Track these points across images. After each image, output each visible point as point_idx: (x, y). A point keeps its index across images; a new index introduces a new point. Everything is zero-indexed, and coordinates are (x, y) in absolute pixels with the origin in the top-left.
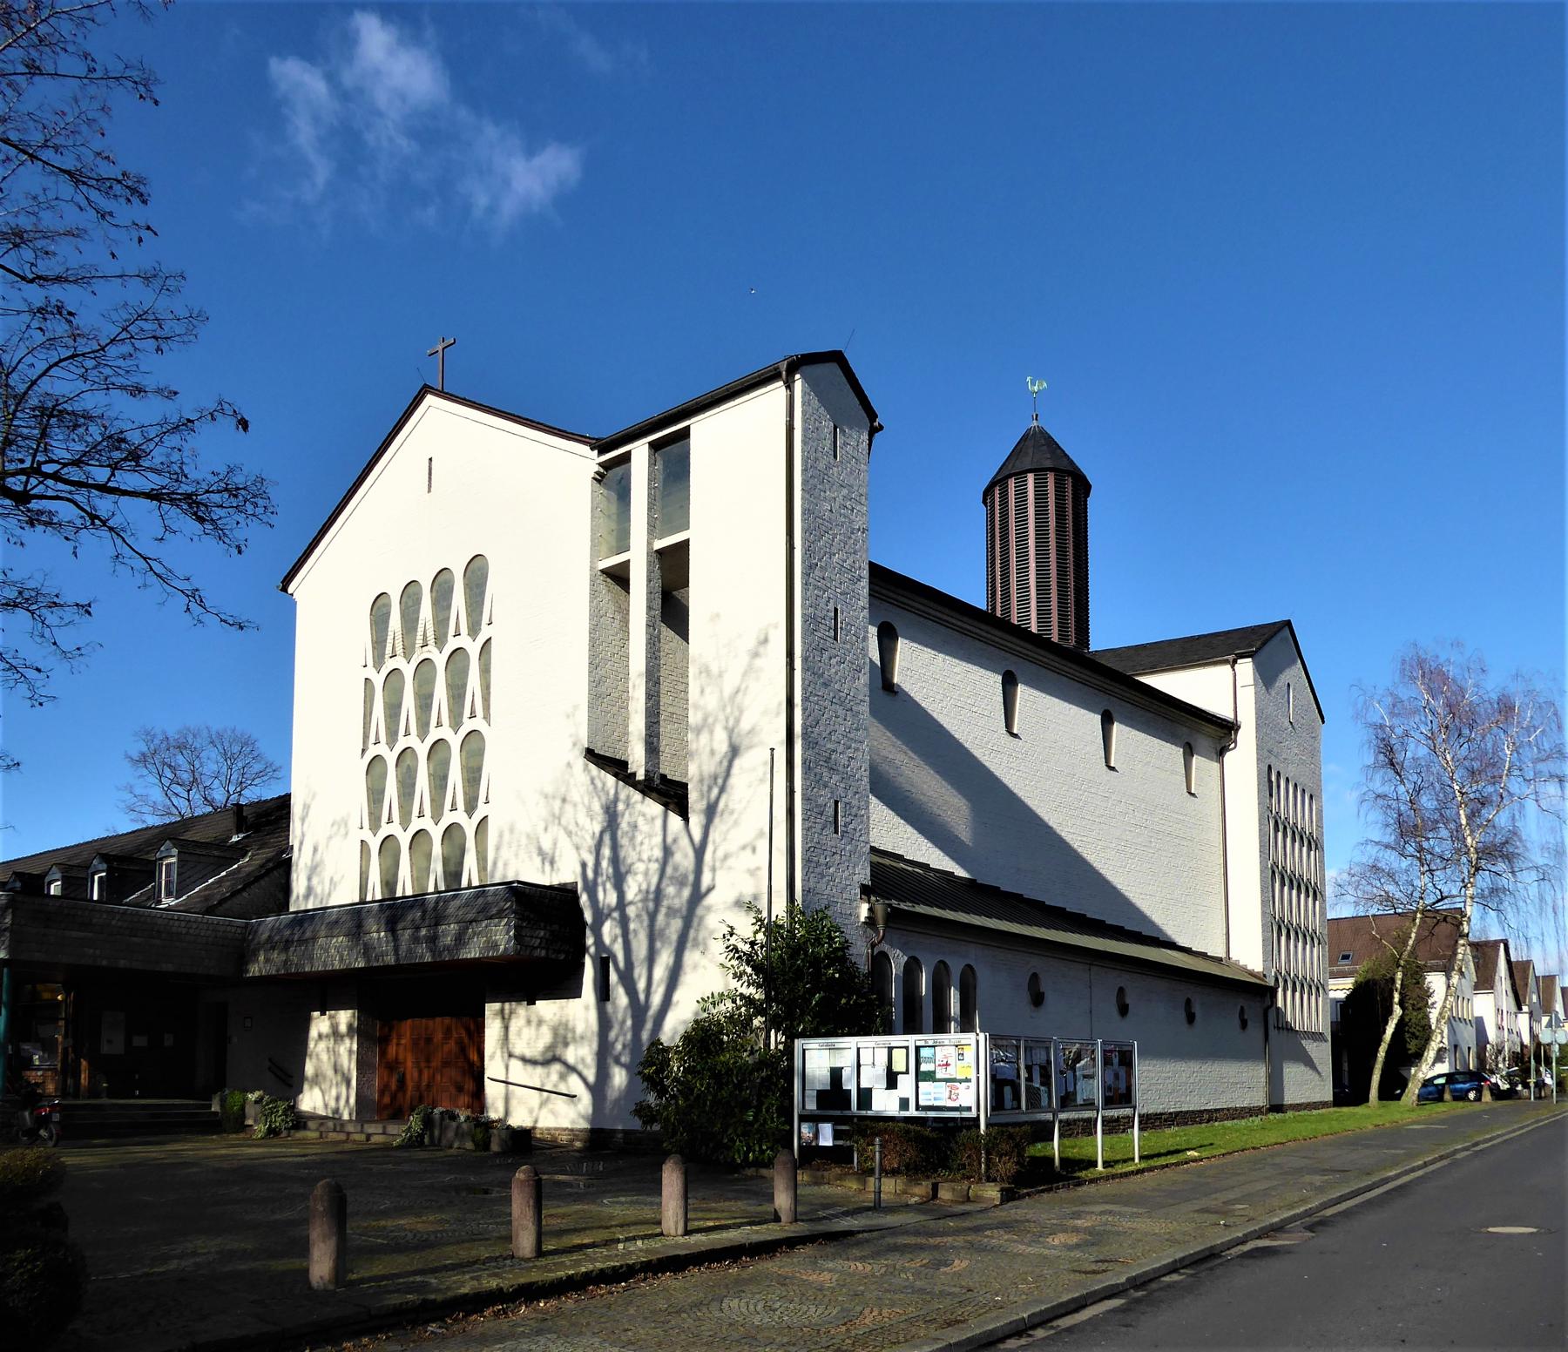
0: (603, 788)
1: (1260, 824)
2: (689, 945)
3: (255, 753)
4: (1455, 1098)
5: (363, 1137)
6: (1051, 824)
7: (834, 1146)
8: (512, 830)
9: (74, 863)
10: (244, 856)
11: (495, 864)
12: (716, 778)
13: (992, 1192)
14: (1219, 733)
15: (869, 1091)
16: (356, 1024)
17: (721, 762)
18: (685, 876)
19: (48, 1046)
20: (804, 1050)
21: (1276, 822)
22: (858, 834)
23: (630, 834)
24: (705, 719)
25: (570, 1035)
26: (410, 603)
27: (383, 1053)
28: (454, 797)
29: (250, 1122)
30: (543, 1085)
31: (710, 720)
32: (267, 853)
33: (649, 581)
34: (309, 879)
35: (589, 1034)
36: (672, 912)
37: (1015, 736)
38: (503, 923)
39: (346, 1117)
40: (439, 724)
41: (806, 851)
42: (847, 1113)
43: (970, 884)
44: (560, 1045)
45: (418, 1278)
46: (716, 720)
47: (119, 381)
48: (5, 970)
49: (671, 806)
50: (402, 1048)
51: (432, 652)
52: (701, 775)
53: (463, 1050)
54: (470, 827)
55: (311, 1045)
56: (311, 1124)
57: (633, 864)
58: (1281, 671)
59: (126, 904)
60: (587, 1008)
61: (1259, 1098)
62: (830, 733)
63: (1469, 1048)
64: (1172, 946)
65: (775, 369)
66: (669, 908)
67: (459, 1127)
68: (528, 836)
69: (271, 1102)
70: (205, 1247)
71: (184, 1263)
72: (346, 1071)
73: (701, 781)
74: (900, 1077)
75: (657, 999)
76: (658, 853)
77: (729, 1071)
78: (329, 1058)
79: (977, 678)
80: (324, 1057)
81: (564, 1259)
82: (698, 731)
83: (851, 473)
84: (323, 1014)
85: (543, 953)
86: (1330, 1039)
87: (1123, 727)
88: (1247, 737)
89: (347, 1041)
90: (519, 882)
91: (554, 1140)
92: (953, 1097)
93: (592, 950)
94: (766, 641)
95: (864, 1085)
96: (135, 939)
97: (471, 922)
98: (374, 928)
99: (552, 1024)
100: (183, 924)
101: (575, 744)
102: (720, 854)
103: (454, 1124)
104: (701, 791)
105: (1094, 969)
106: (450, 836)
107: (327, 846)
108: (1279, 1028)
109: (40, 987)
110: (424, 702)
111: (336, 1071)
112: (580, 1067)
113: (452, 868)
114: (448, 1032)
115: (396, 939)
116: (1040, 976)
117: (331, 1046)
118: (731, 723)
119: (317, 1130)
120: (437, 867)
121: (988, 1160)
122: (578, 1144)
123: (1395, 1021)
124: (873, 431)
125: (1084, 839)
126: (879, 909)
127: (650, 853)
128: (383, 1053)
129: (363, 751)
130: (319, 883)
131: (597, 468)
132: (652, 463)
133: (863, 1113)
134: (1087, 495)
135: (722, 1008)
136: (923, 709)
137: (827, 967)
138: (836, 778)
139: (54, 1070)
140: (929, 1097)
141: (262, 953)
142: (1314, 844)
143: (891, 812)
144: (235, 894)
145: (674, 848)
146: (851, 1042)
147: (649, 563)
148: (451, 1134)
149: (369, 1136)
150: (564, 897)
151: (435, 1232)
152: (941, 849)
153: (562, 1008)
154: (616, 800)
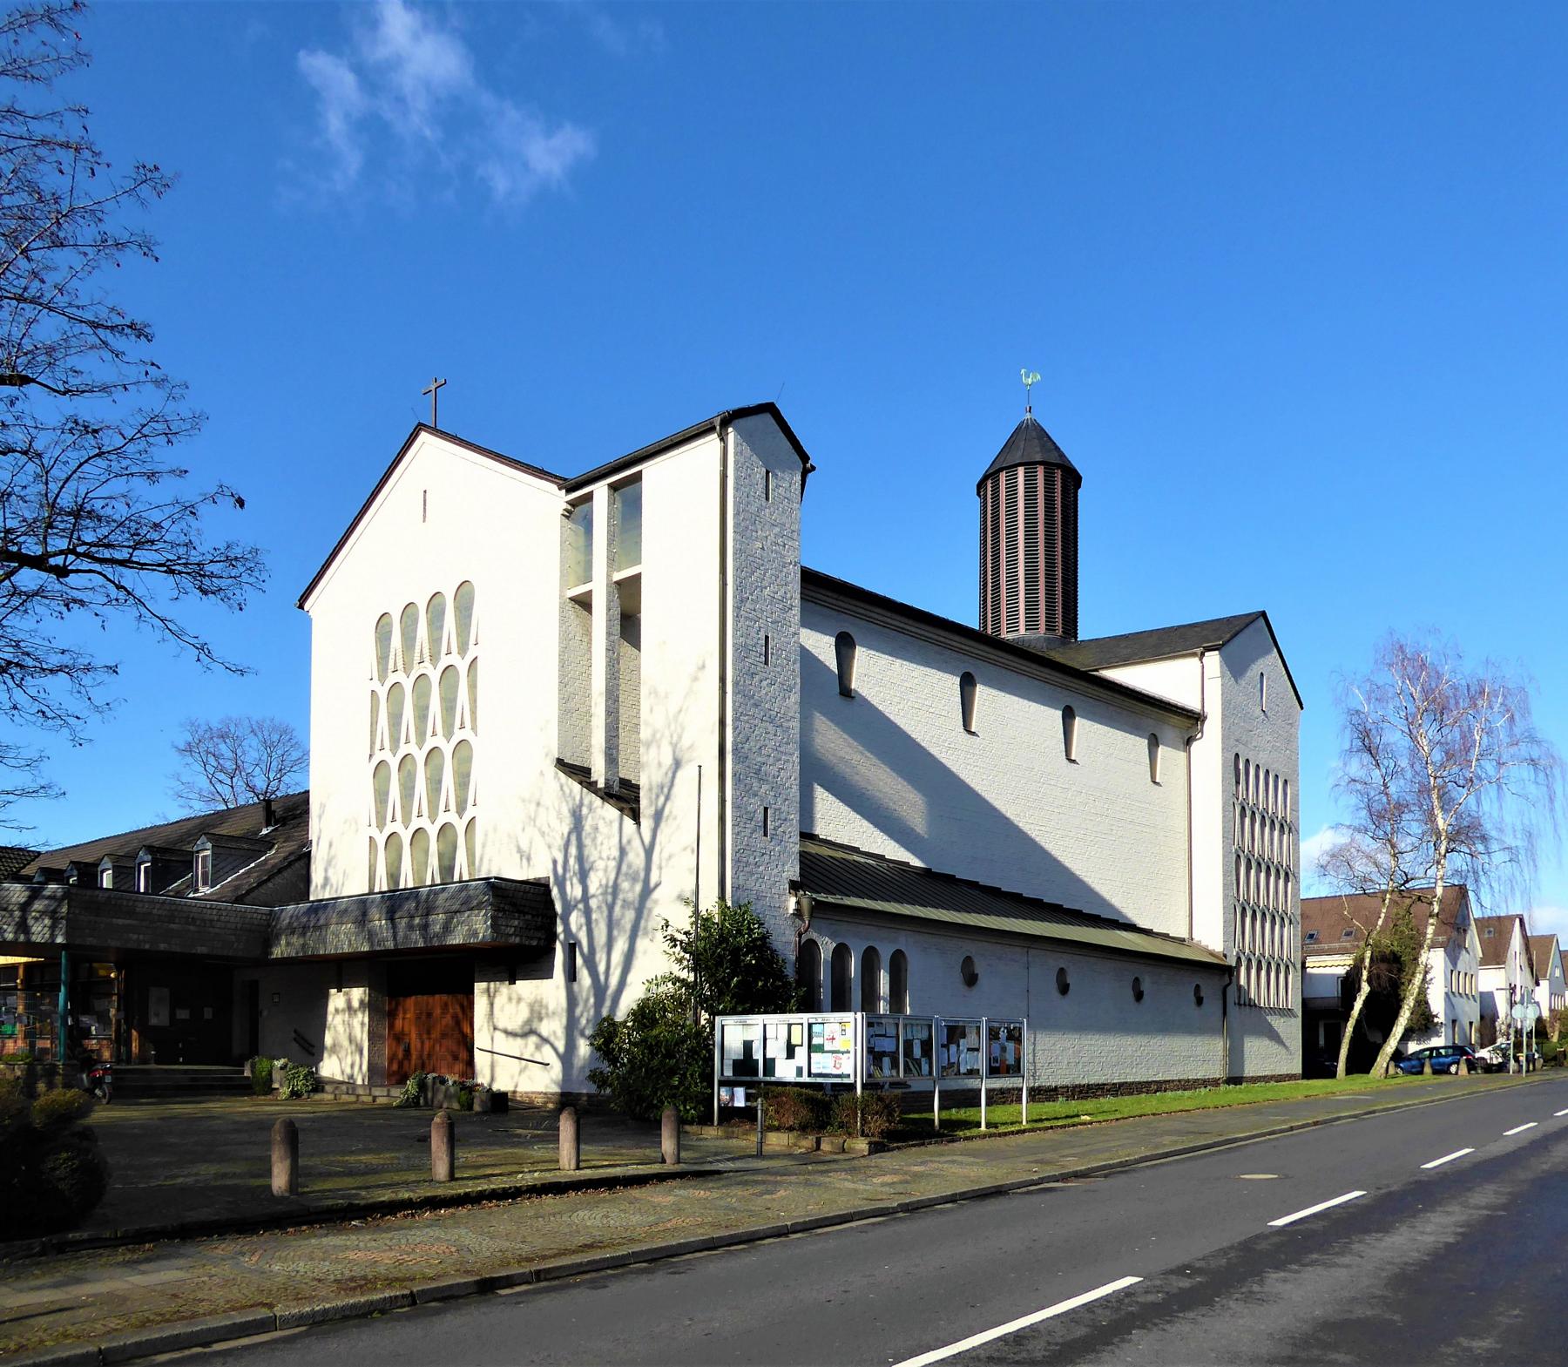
1: (1224, 810)
2: (640, 933)
3: (293, 742)
4: (1435, 1072)
5: (370, 1099)
6: (1008, 815)
7: (746, 1106)
8: (495, 830)
9: (123, 853)
10: (270, 849)
11: (481, 859)
12: (662, 788)
13: (862, 1145)
14: (1189, 721)
15: (773, 1060)
16: (367, 999)
17: (666, 773)
18: (637, 873)
19: (103, 1018)
20: (723, 1026)
21: (1243, 808)
22: (788, 836)
23: (592, 835)
24: (654, 735)
25: (543, 1011)
26: (410, 623)
29: (276, 1085)
31: (658, 736)
32: (291, 846)
33: (609, 609)
34: (326, 870)
35: (559, 1010)
36: (626, 905)
37: (973, 734)
38: (482, 914)
39: (359, 1082)
40: (434, 734)
41: (735, 852)
42: (755, 1079)
43: (927, 873)
44: (536, 1020)
45: (354, 1192)
46: (662, 736)
47: (134, 469)
48: (63, 953)
49: (626, 812)
50: (407, 1021)
51: (427, 668)
52: (650, 784)
53: (458, 1023)
54: (460, 826)
55: (330, 1018)
56: (328, 1088)
57: (594, 862)
58: (1253, 661)
59: (162, 895)
60: (558, 987)
61: (1217, 1070)
63: (1471, 1023)
64: (1131, 927)
65: (711, 423)
67: (447, 1089)
68: (509, 836)
70: (207, 1171)
71: (188, 1180)
72: (359, 1042)
73: (650, 789)
74: (797, 1048)
75: (614, 981)
76: (615, 853)
77: (658, 1044)
79: (935, 681)
81: (470, 1183)
82: (648, 745)
83: (784, 512)
84: (340, 991)
85: (517, 940)
86: (1300, 1014)
87: (1085, 721)
88: (1213, 729)
89: (360, 1015)
91: (532, 1102)
92: (838, 1066)
93: (562, 937)
95: (769, 1056)
96: (172, 926)
97: (456, 912)
98: (377, 917)
100: (215, 912)
101: (547, 755)
102: (665, 855)
103: (443, 1088)
104: (650, 798)
105: (1032, 952)
108: (1240, 1004)
109: (95, 965)
110: (422, 714)
111: (351, 1041)
112: (552, 1039)
113: (446, 863)
114: (445, 1007)
115: (394, 927)
116: (975, 960)
117: (346, 1019)
118: (675, 738)
120: (434, 861)
121: (863, 1119)
122: (551, 1106)
123: (1363, 998)
124: (805, 473)
125: (1043, 829)
126: (805, 903)
128: (391, 1026)
132: (611, 503)
133: (768, 1079)
135: (662, 989)
136: (880, 712)
137: (746, 955)
138: (765, 787)
139: (110, 1039)
142: (1287, 827)
143: (846, 808)
144: (260, 884)
146: (758, 1019)
147: (609, 593)
149: (375, 1098)
150: (539, 890)
151: (383, 1165)
152: (897, 841)
153: (537, 987)
154: (581, 804)
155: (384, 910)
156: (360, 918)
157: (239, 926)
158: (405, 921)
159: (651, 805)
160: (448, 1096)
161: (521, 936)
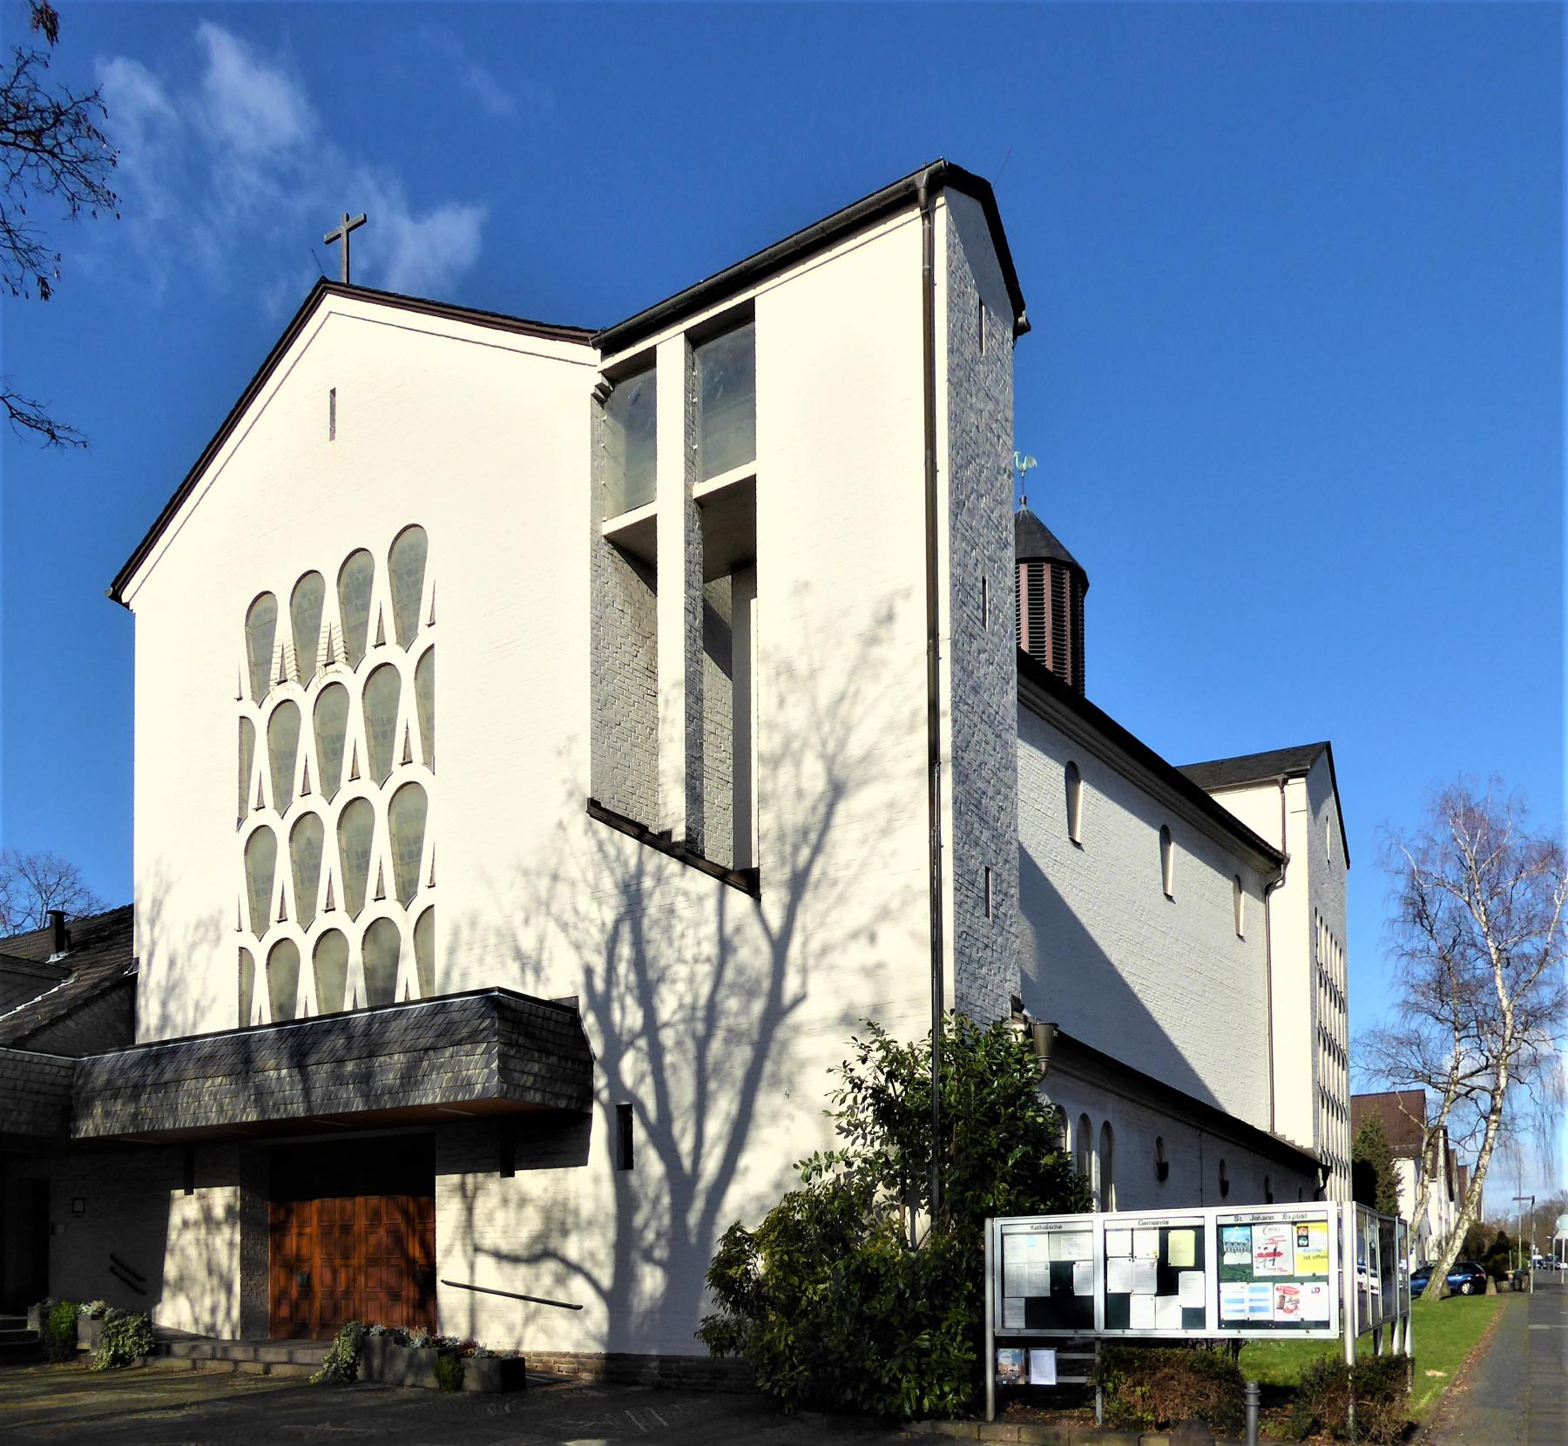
0: (618, 858)
2: (763, 1084)
3: (77, 887)
7: (1059, 1384)
8: (473, 924)
10: (67, 977)
17: (814, 808)
22: (1008, 923)
23: (663, 923)
24: (787, 745)
25: (570, 1220)
26: (306, 605)
27: (278, 1248)
28: (380, 875)
30: (529, 1291)
31: (796, 745)
33: (688, 543)
34: (164, 1004)
35: (601, 1218)
36: (734, 1036)
38: (479, 1051)
50: (306, 1238)
51: (341, 672)
52: (781, 829)
53: (399, 1242)
54: (405, 922)
55: (173, 1235)
56: (178, 1348)
57: (669, 966)
60: (597, 1180)
62: (980, 766)
66: (730, 1030)
68: (499, 933)
69: (116, 1317)
72: (225, 1272)
73: (781, 838)
74: (1182, 1276)
75: (711, 1165)
76: (710, 949)
78: (200, 1254)
79: (1040, 766)
80: (192, 1252)
84: (189, 1192)
85: (538, 1098)
87: (1180, 849)
88: (1297, 873)
90: (501, 990)
92: (1288, 1305)
93: (605, 1095)
94: (890, 618)
97: (426, 1050)
98: (272, 1063)
99: (541, 1203)
101: (570, 794)
102: (815, 945)
103: (406, 1351)
104: (781, 853)
106: (375, 941)
107: (189, 958)
110: (331, 747)
111: (210, 1272)
112: (588, 1266)
113: (380, 983)
114: (375, 1217)
115: (305, 1078)
118: (831, 746)
119: (187, 1356)
122: (586, 1377)
127: (695, 950)
128: (278, 1248)
129: (240, 821)
130: (178, 1010)
131: (600, 379)
132: (690, 366)
134: (1084, 592)
140: (1239, 1306)
141: (98, 1103)
144: (55, 1021)
145: (736, 941)
147: (687, 515)
148: (400, 1366)
150: (565, 1012)
153: (558, 1180)
155: (285, 1053)
156: (240, 1067)
157: (20, 1084)
158: (326, 1068)
159: (783, 864)
160: (414, 1365)
161: (544, 1091)
